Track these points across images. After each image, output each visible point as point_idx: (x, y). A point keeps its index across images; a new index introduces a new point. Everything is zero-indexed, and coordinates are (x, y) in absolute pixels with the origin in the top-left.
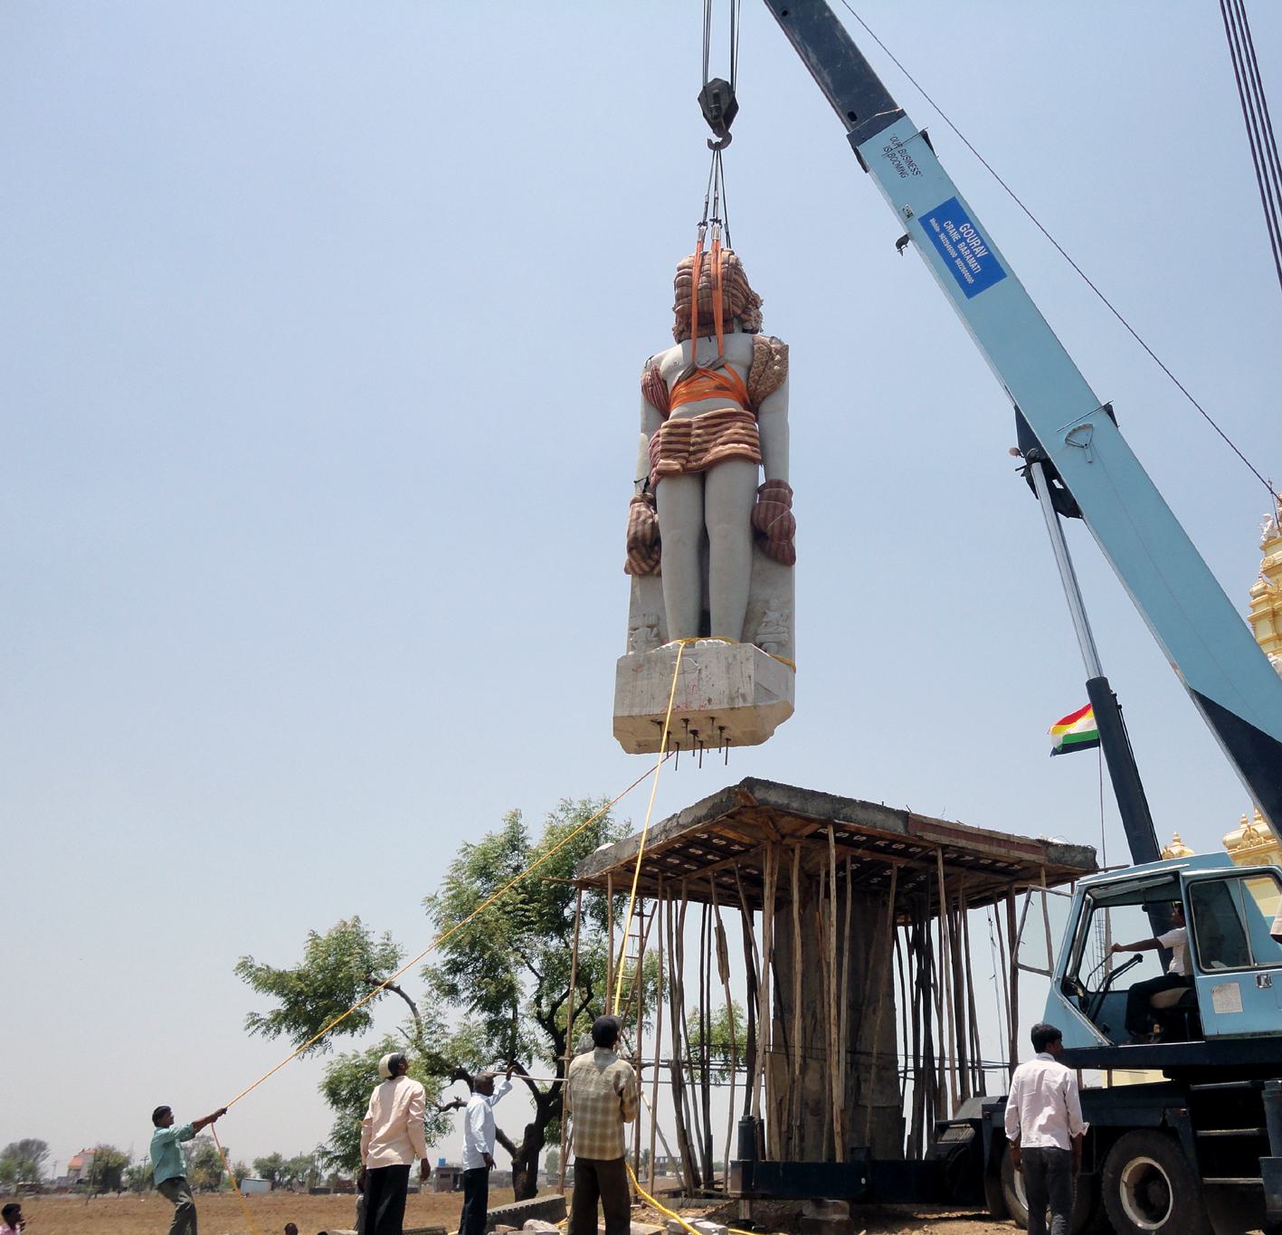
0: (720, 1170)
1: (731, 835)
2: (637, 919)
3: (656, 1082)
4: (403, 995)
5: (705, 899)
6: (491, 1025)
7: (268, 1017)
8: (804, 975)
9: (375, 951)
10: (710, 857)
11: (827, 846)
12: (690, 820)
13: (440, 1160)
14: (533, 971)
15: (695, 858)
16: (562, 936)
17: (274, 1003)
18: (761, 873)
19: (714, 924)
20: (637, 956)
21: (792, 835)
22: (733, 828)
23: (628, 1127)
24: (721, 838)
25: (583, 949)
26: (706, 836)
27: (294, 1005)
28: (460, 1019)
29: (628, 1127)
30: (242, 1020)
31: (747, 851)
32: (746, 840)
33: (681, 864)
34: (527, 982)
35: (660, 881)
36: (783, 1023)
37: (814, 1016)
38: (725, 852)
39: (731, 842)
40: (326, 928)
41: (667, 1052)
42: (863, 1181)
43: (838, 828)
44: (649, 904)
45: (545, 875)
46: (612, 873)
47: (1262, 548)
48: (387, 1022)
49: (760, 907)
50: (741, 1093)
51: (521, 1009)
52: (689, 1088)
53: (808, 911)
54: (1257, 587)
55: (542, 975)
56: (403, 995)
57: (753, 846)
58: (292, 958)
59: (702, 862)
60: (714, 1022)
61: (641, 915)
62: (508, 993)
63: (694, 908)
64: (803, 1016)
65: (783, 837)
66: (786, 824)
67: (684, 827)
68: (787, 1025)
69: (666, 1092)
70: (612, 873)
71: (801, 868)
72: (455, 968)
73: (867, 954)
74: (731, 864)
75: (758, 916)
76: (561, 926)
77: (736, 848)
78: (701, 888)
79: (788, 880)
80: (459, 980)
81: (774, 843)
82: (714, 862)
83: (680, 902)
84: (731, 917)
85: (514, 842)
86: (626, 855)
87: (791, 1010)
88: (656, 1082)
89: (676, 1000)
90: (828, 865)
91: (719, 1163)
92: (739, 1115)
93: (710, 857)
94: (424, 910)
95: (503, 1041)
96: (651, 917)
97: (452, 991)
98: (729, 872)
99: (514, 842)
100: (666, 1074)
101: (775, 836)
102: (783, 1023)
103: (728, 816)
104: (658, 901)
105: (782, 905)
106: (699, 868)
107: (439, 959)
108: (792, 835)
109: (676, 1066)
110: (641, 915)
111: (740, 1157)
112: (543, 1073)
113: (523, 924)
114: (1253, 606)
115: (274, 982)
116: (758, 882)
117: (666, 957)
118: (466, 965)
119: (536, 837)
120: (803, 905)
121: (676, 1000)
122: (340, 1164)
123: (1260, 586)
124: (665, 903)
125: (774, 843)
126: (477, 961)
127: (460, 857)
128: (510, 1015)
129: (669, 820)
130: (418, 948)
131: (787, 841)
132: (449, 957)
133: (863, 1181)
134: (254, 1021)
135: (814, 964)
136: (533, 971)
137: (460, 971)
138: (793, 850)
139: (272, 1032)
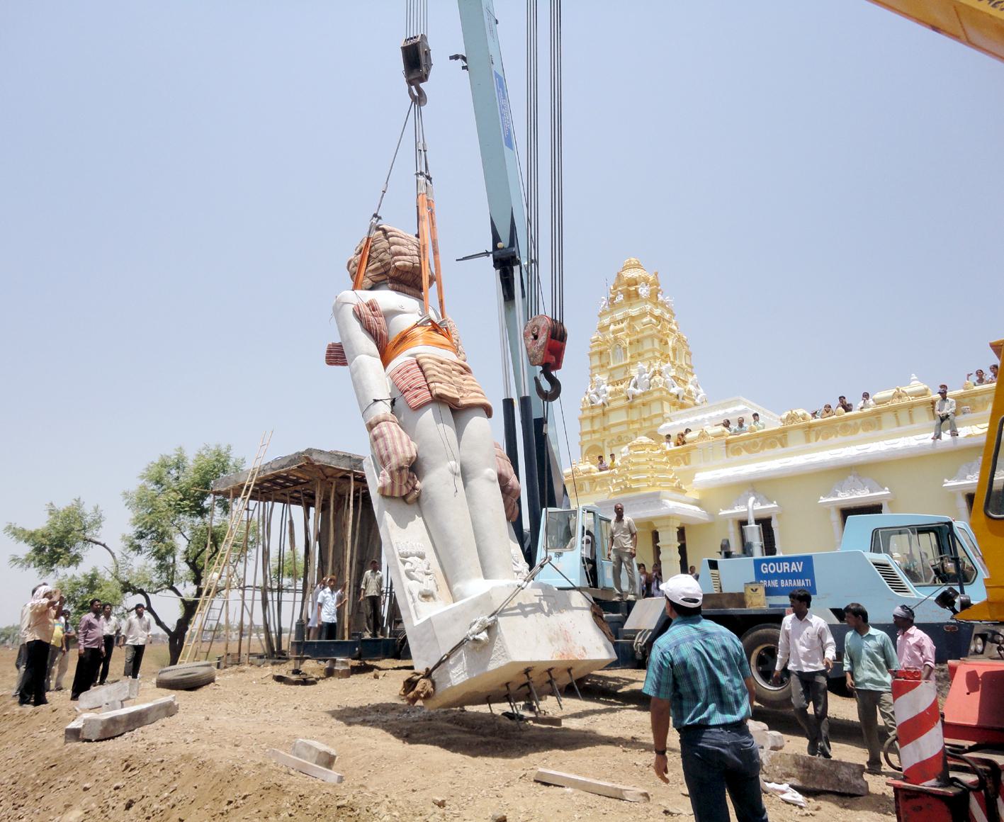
0: (286, 633)
1: (300, 475)
2: (246, 512)
3: (253, 600)
4: (107, 548)
5: (284, 502)
6: (160, 567)
7: (23, 558)
8: (334, 547)
9: (88, 519)
10: (288, 484)
11: (350, 482)
12: (277, 466)
13: (158, 687)
14: (185, 537)
15: (280, 484)
16: (202, 518)
17: (25, 549)
18: (314, 493)
19: (288, 519)
20: (241, 598)
21: (332, 476)
22: (301, 472)
23: (240, 566)
24: (294, 476)
25: (215, 524)
26: (285, 475)
27: (39, 550)
28: (142, 564)
29: (240, 566)
30: (8, 558)
31: (308, 482)
32: (308, 478)
33: (272, 486)
34: (181, 543)
35: (259, 494)
36: (322, 570)
37: (339, 566)
38: (296, 483)
39: (299, 478)
40: (62, 504)
41: (260, 582)
42: (357, 649)
43: (355, 474)
44: (252, 503)
45: (193, 486)
46: (233, 489)
47: (599, 316)
48: (94, 561)
49: (313, 505)
50: (298, 605)
51: (178, 558)
52: (270, 603)
53: (339, 513)
54: (594, 337)
55: (190, 539)
56: (107, 548)
57: (311, 481)
58: (39, 522)
59: (283, 486)
60: (286, 558)
61: (248, 509)
62: (171, 550)
63: (278, 506)
64: (333, 568)
65: (327, 477)
66: (329, 472)
67: (274, 469)
68: (324, 570)
69: (258, 605)
70: (233, 489)
71: (336, 492)
72: (141, 536)
73: (369, 535)
74: (299, 488)
75: (312, 510)
76: (202, 512)
77: (302, 481)
78: (283, 497)
79: (329, 497)
80: (143, 543)
81: (322, 480)
82: (290, 487)
83: (270, 503)
84: (297, 511)
85: (179, 465)
86: (241, 481)
87: (327, 563)
88: (253, 600)
89: (266, 558)
90: (350, 491)
91: (286, 629)
92: (297, 618)
93: (288, 484)
94: (122, 497)
95: (168, 576)
96: (254, 510)
97: (139, 548)
98: (296, 491)
99: (179, 465)
100: (259, 595)
101: (322, 477)
102: (322, 570)
103: (298, 467)
104: (258, 502)
105: (324, 508)
106: (281, 489)
107: (131, 531)
108: (332, 476)
109: (265, 590)
110: (248, 509)
111: (296, 639)
112: (189, 590)
113: (180, 511)
114: (591, 348)
115: (30, 537)
116: (313, 497)
117: (261, 523)
118: (147, 535)
119: (191, 463)
120: (336, 509)
121: (266, 558)
122: (50, 626)
123: (595, 337)
124: (262, 503)
125: (322, 480)
126: (152, 533)
127: (145, 472)
128: (171, 561)
129: (266, 465)
130: (117, 524)
131: (329, 479)
132: (140, 529)
133: (357, 649)
134: (15, 560)
135: (340, 541)
136: (185, 537)
137: (142, 537)
138: (332, 483)
139: (25, 566)
